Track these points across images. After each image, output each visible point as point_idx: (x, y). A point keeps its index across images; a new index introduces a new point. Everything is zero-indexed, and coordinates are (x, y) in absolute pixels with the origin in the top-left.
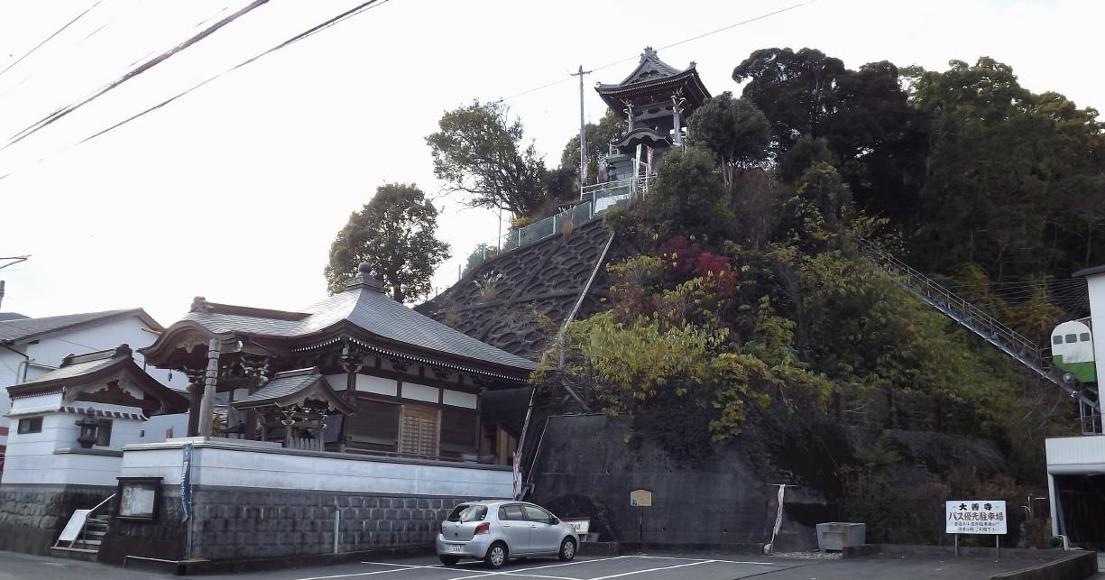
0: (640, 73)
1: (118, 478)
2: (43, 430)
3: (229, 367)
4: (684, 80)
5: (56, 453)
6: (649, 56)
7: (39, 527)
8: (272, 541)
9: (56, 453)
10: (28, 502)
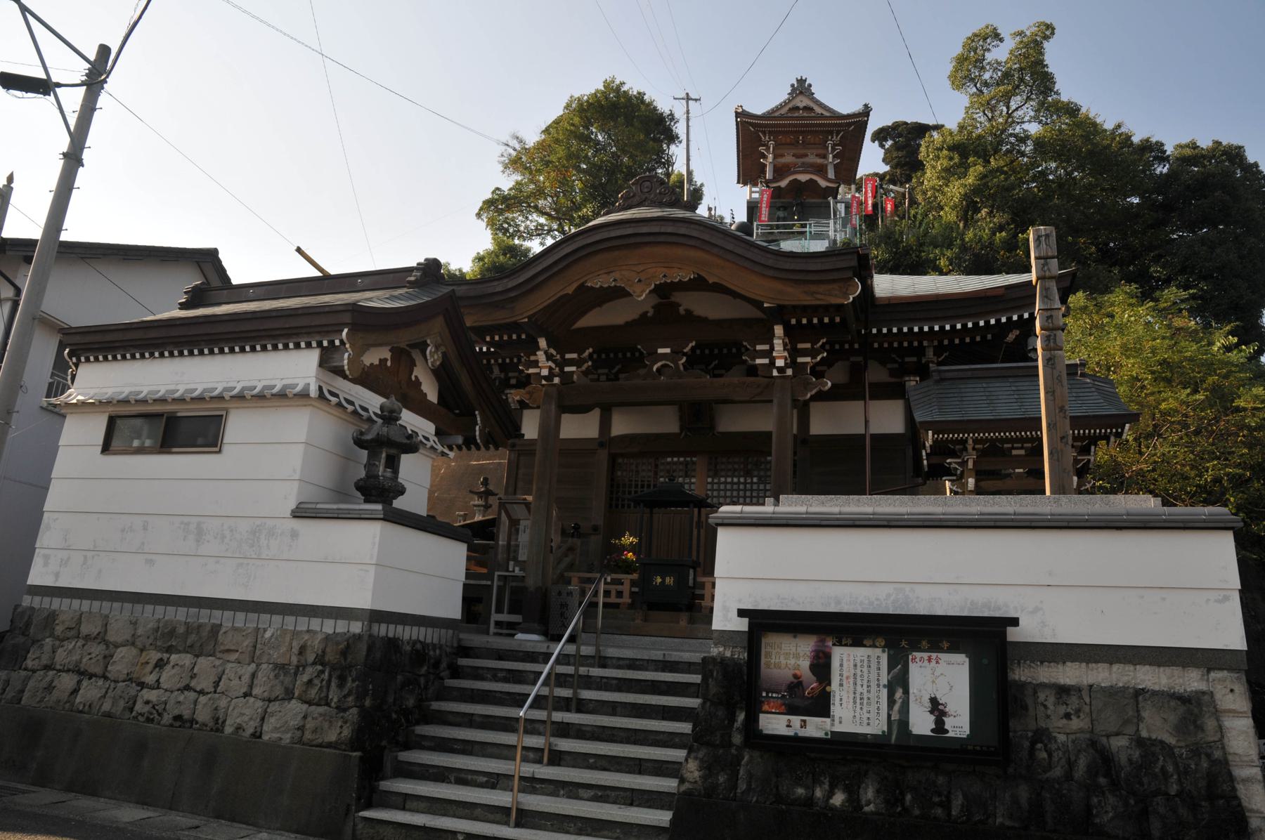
0: (790, 106)
1: (742, 613)
2: (225, 448)
3: (676, 353)
4: (849, 125)
5: (301, 513)
6: (801, 88)
7: (257, 735)
8: (256, 691)
9: (301, 513)
10: (170, 650)
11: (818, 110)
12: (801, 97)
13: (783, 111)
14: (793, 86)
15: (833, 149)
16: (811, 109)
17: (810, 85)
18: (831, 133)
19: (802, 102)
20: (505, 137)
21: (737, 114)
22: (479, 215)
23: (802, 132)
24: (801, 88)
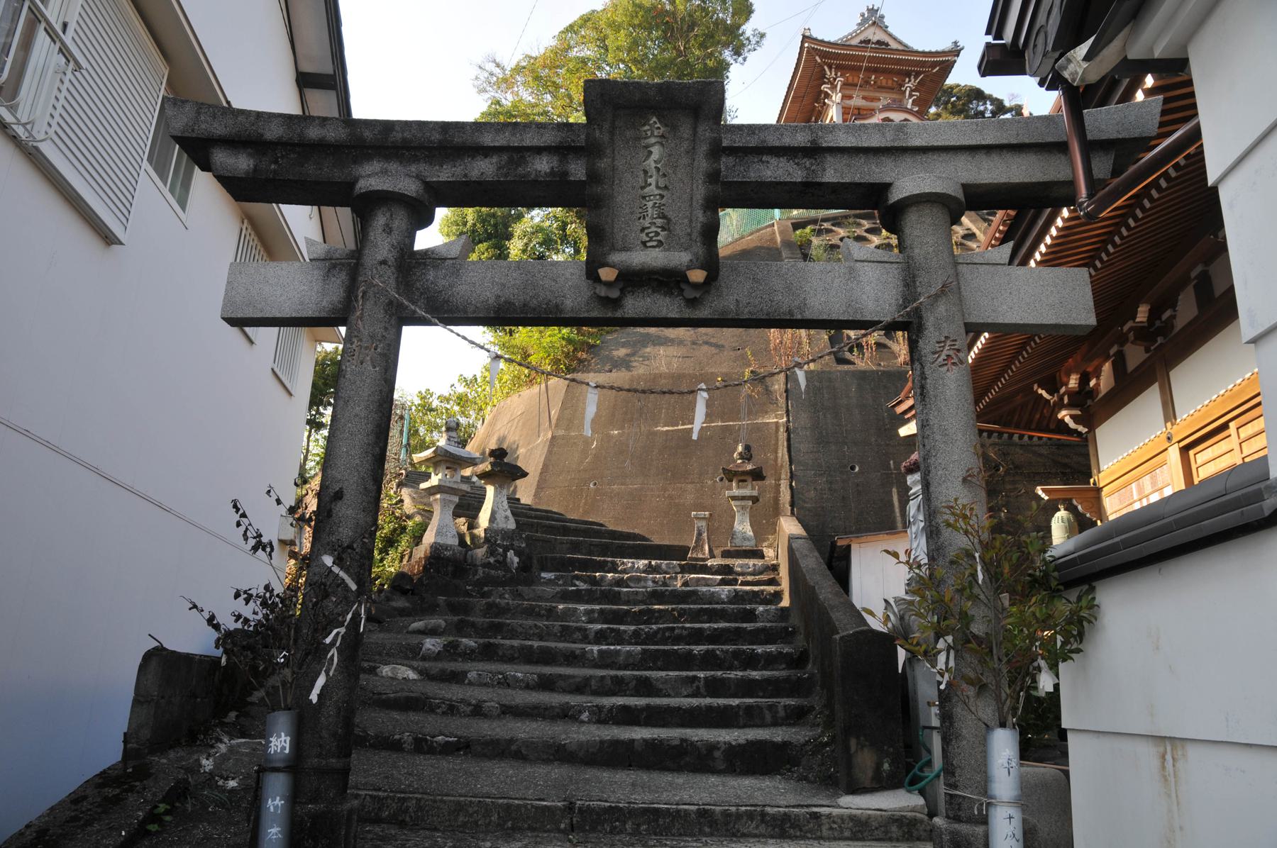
0: (862, 37)
4: (934, 64)
6: (873, 18)
11: (894, 45)
12: (872, 29)
13: (855, 42)
14: (863, 15)
15: (911, 96)
16: (887, 45)
17: (882, 17)
18: (908, 74)
19: (875, 35)
20: (479, 60)
21: (805, 38)
22: (527, 56)
23: (875, 70)
24: (873, 18)
